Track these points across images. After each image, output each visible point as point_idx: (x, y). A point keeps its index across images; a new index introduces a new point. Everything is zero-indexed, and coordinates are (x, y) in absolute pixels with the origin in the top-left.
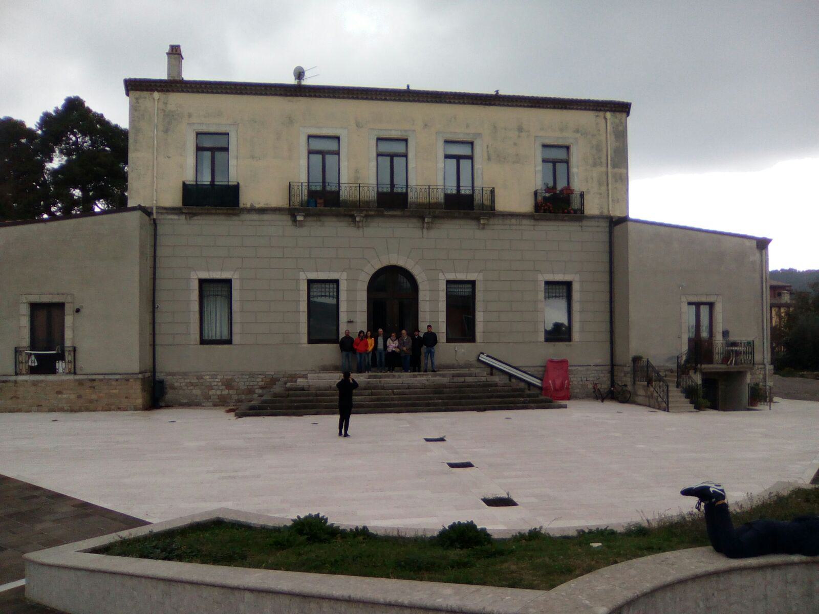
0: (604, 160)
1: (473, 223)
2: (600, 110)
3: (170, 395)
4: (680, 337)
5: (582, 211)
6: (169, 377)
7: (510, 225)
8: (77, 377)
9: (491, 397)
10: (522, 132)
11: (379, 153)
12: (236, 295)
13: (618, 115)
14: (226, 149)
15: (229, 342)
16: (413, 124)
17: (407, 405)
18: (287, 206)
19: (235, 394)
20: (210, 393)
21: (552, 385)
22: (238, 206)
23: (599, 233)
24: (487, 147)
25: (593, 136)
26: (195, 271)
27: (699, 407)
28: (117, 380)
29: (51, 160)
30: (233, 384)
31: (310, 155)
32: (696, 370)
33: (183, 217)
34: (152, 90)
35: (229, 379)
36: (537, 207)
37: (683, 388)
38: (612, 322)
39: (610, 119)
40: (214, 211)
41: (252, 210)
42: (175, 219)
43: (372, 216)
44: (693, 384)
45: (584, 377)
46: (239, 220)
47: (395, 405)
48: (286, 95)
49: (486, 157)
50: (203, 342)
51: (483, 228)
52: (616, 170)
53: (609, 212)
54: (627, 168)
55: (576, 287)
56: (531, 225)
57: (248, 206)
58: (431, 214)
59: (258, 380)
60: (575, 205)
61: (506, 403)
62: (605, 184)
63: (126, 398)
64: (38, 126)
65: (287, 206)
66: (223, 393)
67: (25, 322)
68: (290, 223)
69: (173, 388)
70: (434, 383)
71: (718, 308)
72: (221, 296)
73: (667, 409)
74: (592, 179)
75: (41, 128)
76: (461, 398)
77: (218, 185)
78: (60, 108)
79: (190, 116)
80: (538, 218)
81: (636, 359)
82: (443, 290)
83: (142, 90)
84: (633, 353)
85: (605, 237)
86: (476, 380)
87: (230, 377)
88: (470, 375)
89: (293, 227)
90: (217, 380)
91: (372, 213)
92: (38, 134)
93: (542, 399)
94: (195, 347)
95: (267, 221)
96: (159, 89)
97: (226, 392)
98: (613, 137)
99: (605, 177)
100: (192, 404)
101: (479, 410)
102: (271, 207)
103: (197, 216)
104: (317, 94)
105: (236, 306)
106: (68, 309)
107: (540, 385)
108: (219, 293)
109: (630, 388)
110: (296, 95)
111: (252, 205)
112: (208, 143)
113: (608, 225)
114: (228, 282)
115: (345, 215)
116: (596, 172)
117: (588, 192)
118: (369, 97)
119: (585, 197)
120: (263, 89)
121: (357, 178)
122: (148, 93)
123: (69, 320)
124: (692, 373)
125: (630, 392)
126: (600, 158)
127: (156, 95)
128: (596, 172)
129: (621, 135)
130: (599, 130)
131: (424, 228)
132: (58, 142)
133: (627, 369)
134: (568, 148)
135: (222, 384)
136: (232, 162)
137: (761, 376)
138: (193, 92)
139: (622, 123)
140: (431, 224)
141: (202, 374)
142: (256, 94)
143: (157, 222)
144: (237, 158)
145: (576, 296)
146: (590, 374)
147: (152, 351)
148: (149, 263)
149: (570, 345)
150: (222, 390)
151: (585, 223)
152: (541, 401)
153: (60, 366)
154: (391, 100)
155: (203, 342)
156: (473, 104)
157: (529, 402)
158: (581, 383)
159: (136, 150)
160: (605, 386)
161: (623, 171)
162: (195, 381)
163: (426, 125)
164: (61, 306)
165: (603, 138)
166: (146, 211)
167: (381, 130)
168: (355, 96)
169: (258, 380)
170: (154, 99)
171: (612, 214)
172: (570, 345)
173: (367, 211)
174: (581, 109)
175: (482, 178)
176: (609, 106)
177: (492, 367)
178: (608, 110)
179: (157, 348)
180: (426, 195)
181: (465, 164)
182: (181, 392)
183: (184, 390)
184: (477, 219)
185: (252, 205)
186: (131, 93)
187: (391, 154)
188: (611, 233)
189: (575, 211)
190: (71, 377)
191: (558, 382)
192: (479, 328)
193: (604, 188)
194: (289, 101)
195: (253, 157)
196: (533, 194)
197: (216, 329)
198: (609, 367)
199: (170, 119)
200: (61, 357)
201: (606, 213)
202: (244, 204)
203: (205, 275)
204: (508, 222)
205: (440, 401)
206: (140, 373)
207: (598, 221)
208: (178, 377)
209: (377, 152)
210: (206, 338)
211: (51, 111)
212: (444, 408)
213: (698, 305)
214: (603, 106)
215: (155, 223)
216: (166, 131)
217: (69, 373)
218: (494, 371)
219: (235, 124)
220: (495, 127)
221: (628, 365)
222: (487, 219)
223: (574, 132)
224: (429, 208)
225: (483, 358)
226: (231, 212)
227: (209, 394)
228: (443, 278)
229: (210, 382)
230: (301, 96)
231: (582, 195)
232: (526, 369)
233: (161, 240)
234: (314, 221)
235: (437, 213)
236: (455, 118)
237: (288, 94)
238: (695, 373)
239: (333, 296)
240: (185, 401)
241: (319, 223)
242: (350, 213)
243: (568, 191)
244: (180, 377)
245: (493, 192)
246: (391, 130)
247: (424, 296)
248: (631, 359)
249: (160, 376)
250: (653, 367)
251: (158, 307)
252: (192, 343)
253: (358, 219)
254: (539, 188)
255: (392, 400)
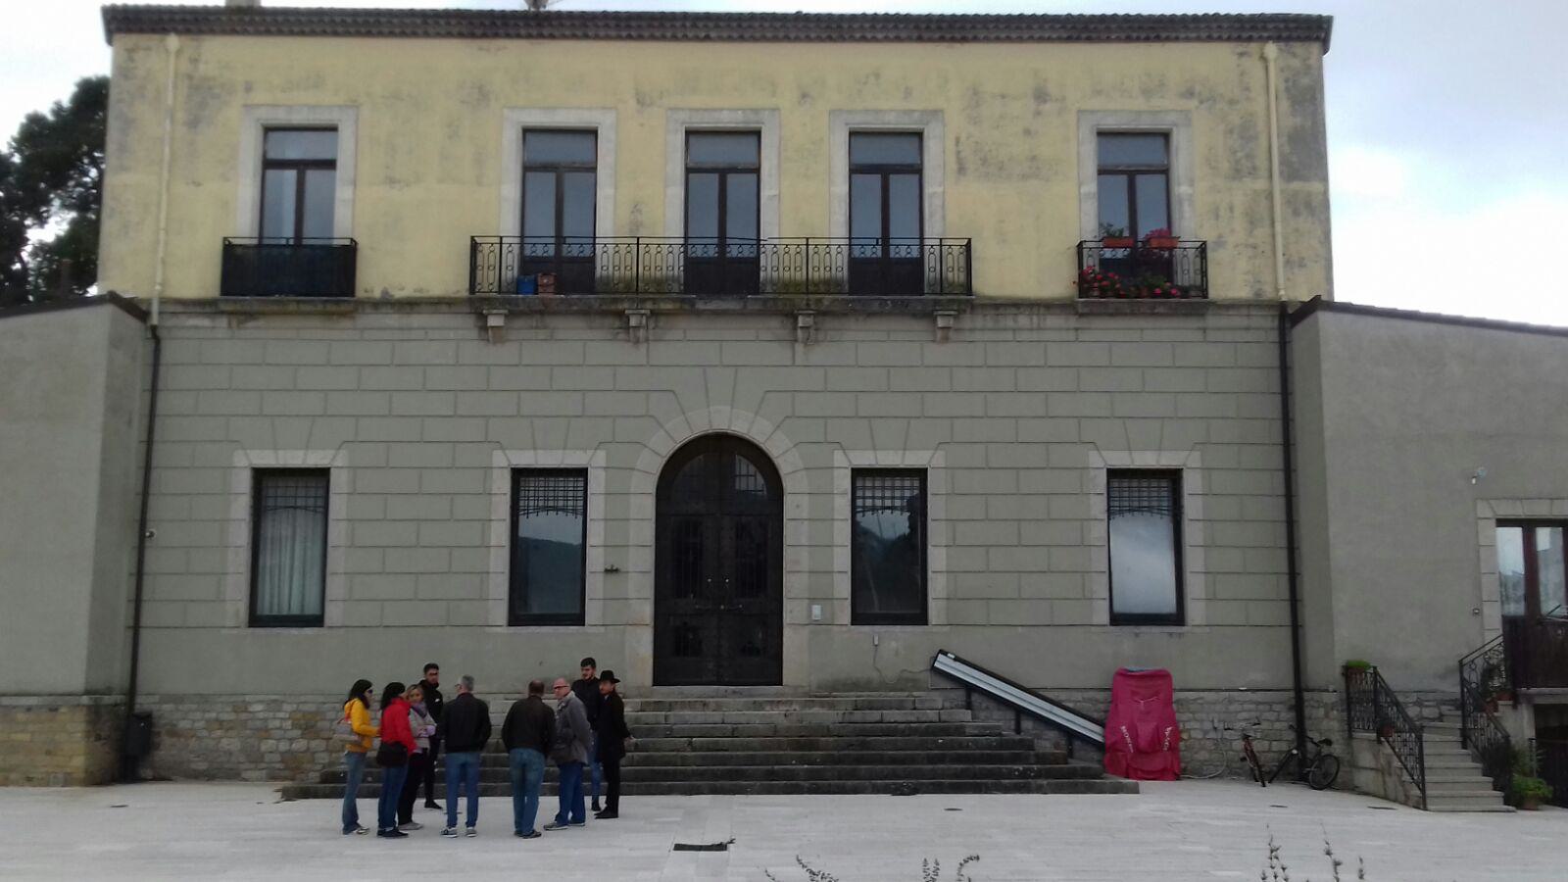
0: (1261, 162)
1: (919, 326)
2: (1250, 39)
3: (167, 750)
4: (1477, 613)
6: (167, 707)
7: (1014, 330)
9: (941, 759)
10: (1045, 101)
11: (691, 165)
12: (338, 506)
13: (1298, 48)
14: (330, 164)
15: (317, 621)
16: (774, 94)
17: (715, 776)
18: (465, 294)
19: (323, 751)
20: (263, 748)
21: (1129, 740)
22: (352, 293)
23: (1258, 344)
24: (958, 141)
25: (1232, 102)
26: (244, 449)
27: (1516, 800)
28: (29, 709)
29: (42, 221)
30: (320, 724)
31: (528, 174)
32: (1516, 700)
33: (223, 322)
34: (165, 31)
35: (310, 713)
36: (1085, 283)
37: (1476, 747)
38: (1293, 575)
39: (1276, 60)
40: (292, 307)
41: (387, 304)
42: (203, 328)
43: (668, 314)
44: (1499, 735)
45: (1219, 721)
46: (355, 329)
47: (686, 776)
48: (472, 36)
49: (952, 165)
50: (256, 620)
51: (946, 339)
52: (1296, 185)
53: (1277, 290)
54: (1325, 179)
55: (1191, 483)
56: (1068, 329)
57: (377, 294)
58: (813, 307)
60: (1185, 276)
61: (975, 777)
62: (1267, 222)
63: (48, 753)
64: (13, 144)
65: (465, 294)
66: (295, 746)
68: (474, 333)
69: (174, 733)
70: (804, 723)
72: (306, 508)
73: (1422, 804)
74: (1231, 209)
75: (18, 150)
76: (859, 760)
77: (312, 247)
78: (66, 102)
79: (248, 88)
80: (1086, 310)
81: (1351, 671)
82: (844, 493)
83: (141, 31)
84: (1342, 655)
85: (1271, 356)
86: (913, 719)
88: (900, 706)
89: (482, 343)
90: (281, 715)
91: (669, 306)
92: (14, 164)
93: (1075, 769)
94: (235, 631)
95: (418, 329)
96: (180, 27)
97: (300, 745)
98: (1285, 104)
99: (1264, 203)
100: (217, 772)
101: (898, 791)
102: (430, 298)
103: (255, 319)
104: (546, 32)
105: (337, 533)
107: (1099, 738)
108: (300, 502)
109: (1337, 749)
110: (496, 36)
111: (385, 292)
112: (294, 148)
113: (1276, 323)
115: (604, 314)
116: (1240, 194)
117: (1220, 243)
118: (669, 34)
119: (1210, 255)
120: (419, 21)
121: (637, 225)
122: (156, 37)
124: (1504, 710)
125: (1336, 758)
126: (1249, 156)
127: (173, 41)
128: (1240, 194)
129: (1308, 98)
130: (1247, 89)
131: (796, 341)
132: (58, 182)
133: (1330, 698)
134: (1166, 136)
135: (293, 725)
136: (343, 193)
138: (258, 33)
139: (1309, 67)
140: (812, 331)
141: (247, 698)
142: (403, 34)
143: (162, 333)
144: (355, 186)
145: (1192, 507)
146: (1237, 712)
147: (130, 640)
148: (137, 432)
150: (292, 740)
151: (1211, 321)
152: (1072, 774)
154: (720, 39)
155: (256, 620)
157: (1039, 775)
158: (1212, 735)
159: (123, 169)
160: (1275, 744)
161: (1315, 186)
163: (804, 96)
165: (1259, 106)
166: (135, 309)
167: (697, 110)
168: (633, 33)
170: (167, 51)
171: (1284, 295)
172: (1180, 635)
173: (654, 301)
175: (944, 217)
176: (1270, 26)
177: (970, 688)
178: (1269, 38)
179: (144, 635)
180: (800, 260)
181: (899, 183)
182: (193, 743)
183: (200, 738)
184: (929, 316)
185: (385, 292)
186: (117, 37)
187: (721, 166)
188: (1284, 344)
189: (1185, 292)
191: (1146, 730)
192: (937, 586)
193: (1262, 233)
194: (481, 49)
195: (391, 181)
196: (1074, 251)
197: (288, 592)
198: (1292, 694)
199: (202, 97)
201: (1269, 294)
202: (366, 291)
204: (1009, 322)
205: (806, 766)
206: (87, 692)
209: (686, 164)
210: (266, 612)
211: (46, 110)
212: (806, 784)
213: (1529, 526)
214: (1253, 28)
215: (155, 336)
216: (193, 124)
218: (975, 697)
219: (354, 105)
220: (976, 93)
221: (1331, 689)
222: (956, 317)
224: (808, 293)
225: (945, 663)
226: (331, 308)
227: (259, 750)
228: (842, 464)
229: (265, 720)
230: (508, 36)
231: (1203, 250)
232: (1062, 696)
233: (169, 377)
234: (532, 328)
235: (826, 303)
236: (877, 76)
237: (479, 32)
238: (1515, 707)
239: (575, 511)
240: (202, 766)
241: (542, 334)
242: (613, 307)
243: (1167, 237)
244: (194, 706)
246: (722, 110)
248: (1338, 671)
249: (143, 703)
250: (1388, 692)
251: (152, 534)
252: (228, 624)
253: (633, 322)
254: (1089, 237)
255: (684, 761)
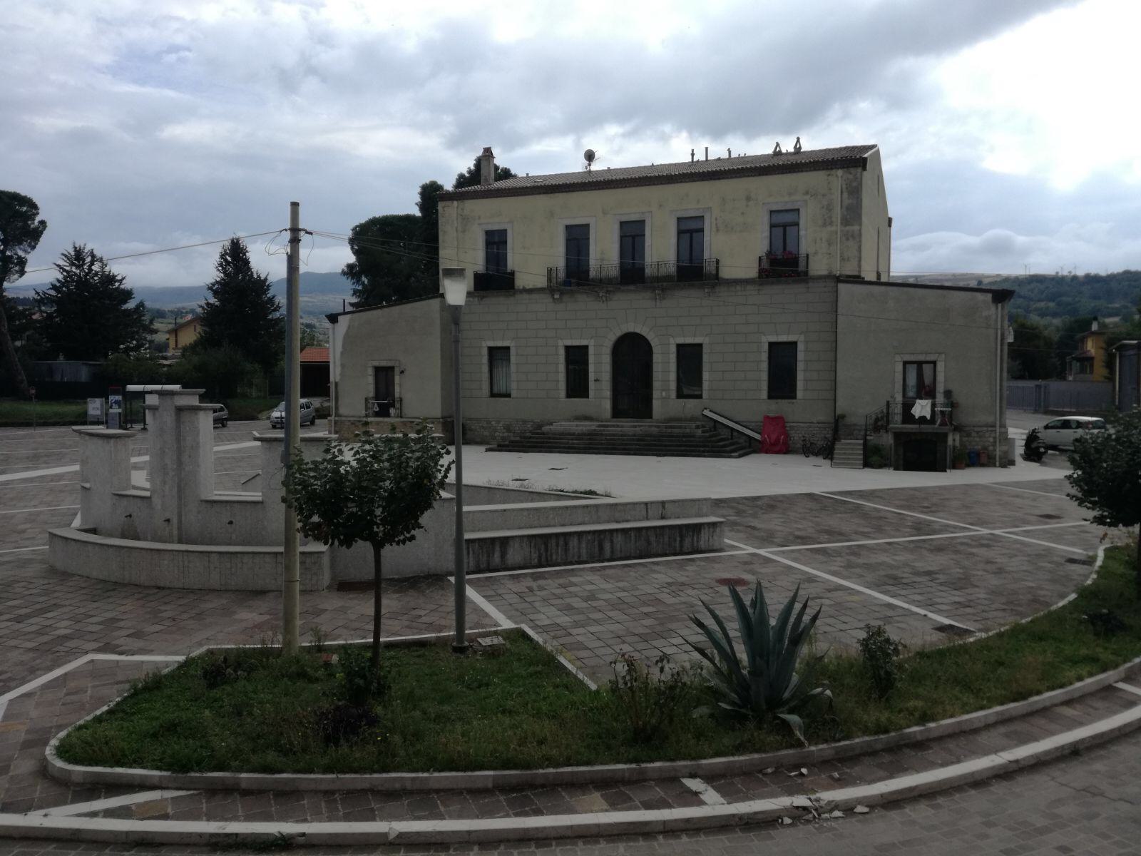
2: (832, 169)
5: (806, 273)
8: (402, 420)
9: (680, 446)
13: (852, 170)
14: (702, 230)
25: (824, 195)
36: (761, 271)
50: (493, 395)
59: (529, 426)
60: (802, 267)
67: (371, 380)
69: (471, 430)
71: (940, 367)
79: (479, 218)
87: (508, 423)
97: (506, 434)
106: (397, 371)
111: (524, 287)
114: (508, 348)
123: (397, 379)
137: (991, 440)
149: (793, 403)
150: (504, 433)
151: (811, 284)
153: (392, 411)
155: (493, 395)
156: (703, 180)
162: (485, 425)
163: (660, 206)
164: (392, 368)
169: (529, 426)
172: (793, 403)
174: (634, 186)
185: (524, 287)
190: (398, 420)
200: (393, 405)
203: (492, 344)
207: (826, 282)
208: (474, 422)
216: (464, 231)
217: (398, 417)
220: (723, 199)
223: (804, 194)
225: (707, 413)
232: (745, 424)
245: (718, 262)
247: (657, 358)
